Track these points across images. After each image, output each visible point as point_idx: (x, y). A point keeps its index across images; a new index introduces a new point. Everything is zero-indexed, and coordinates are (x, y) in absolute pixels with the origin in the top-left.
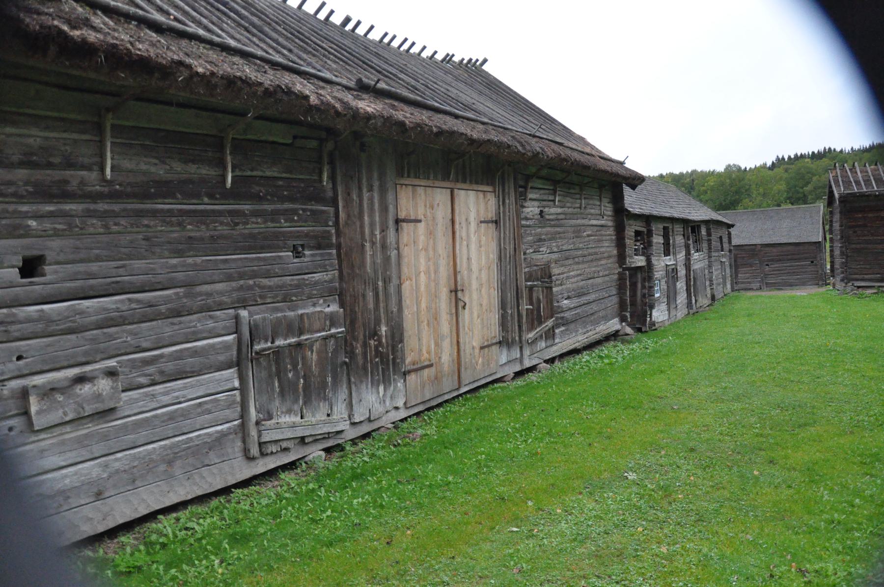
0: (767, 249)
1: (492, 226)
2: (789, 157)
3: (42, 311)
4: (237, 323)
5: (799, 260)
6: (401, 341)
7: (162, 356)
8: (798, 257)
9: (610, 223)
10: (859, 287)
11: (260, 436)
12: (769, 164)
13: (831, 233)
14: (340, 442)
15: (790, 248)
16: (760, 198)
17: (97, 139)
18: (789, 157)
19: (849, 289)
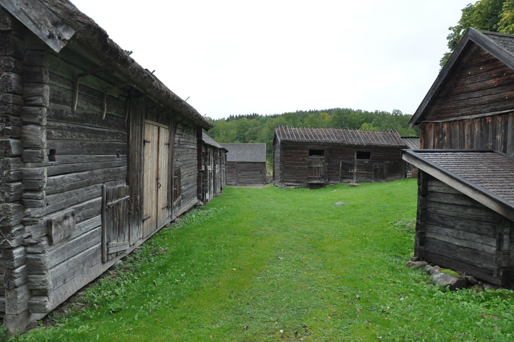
0: (240, 165)
1: (167, 146)
2: (236, 116)
3: (54, 179)
4: (103, 191)
5: (255, 171)
6: (143, 204)
7: (83, 207)
8: (254, 169)
9: (196, 148)
10: (287, 185)
11: (108, 251)
12: (226, 119)
13: (220, 158)
14: (125, 255)
15: (251, 164)
16: (223, 137)
17: (72, 89)
18: (236, 116)
19: (283, 186)
